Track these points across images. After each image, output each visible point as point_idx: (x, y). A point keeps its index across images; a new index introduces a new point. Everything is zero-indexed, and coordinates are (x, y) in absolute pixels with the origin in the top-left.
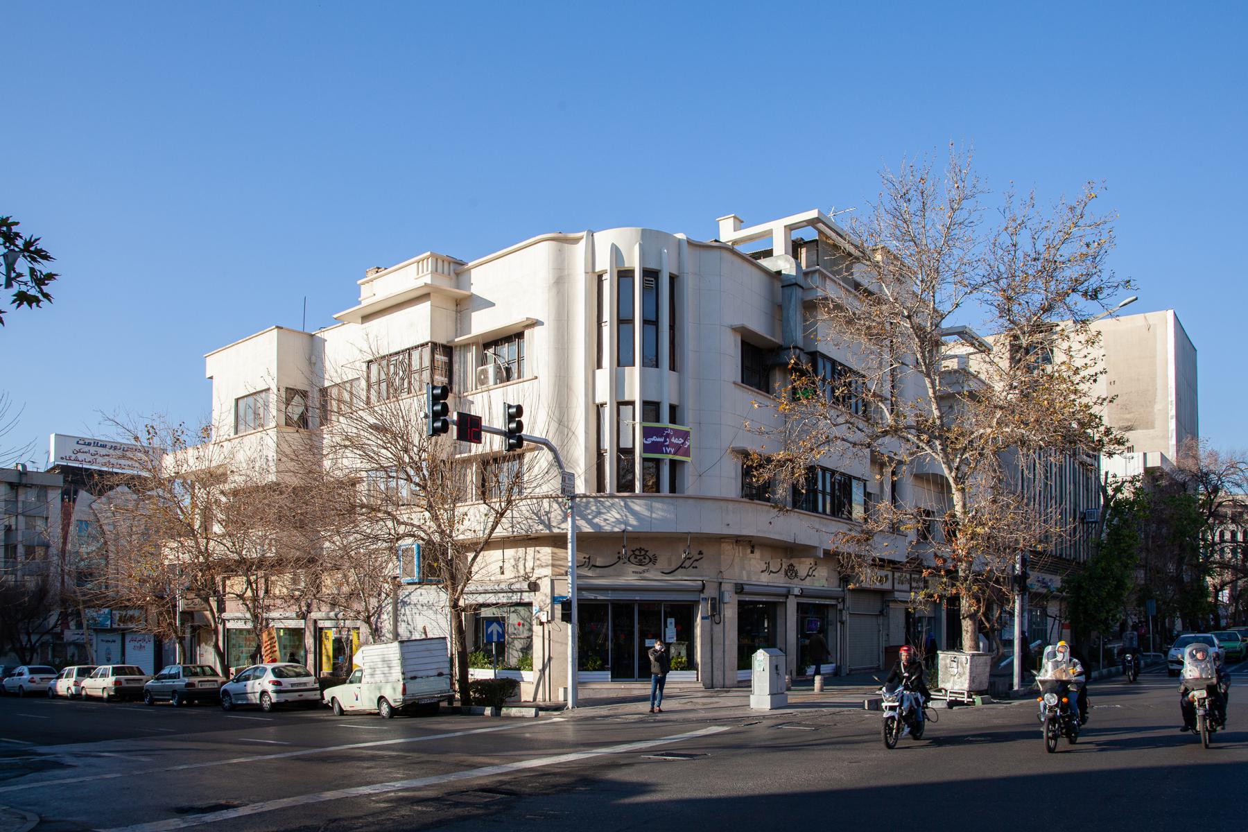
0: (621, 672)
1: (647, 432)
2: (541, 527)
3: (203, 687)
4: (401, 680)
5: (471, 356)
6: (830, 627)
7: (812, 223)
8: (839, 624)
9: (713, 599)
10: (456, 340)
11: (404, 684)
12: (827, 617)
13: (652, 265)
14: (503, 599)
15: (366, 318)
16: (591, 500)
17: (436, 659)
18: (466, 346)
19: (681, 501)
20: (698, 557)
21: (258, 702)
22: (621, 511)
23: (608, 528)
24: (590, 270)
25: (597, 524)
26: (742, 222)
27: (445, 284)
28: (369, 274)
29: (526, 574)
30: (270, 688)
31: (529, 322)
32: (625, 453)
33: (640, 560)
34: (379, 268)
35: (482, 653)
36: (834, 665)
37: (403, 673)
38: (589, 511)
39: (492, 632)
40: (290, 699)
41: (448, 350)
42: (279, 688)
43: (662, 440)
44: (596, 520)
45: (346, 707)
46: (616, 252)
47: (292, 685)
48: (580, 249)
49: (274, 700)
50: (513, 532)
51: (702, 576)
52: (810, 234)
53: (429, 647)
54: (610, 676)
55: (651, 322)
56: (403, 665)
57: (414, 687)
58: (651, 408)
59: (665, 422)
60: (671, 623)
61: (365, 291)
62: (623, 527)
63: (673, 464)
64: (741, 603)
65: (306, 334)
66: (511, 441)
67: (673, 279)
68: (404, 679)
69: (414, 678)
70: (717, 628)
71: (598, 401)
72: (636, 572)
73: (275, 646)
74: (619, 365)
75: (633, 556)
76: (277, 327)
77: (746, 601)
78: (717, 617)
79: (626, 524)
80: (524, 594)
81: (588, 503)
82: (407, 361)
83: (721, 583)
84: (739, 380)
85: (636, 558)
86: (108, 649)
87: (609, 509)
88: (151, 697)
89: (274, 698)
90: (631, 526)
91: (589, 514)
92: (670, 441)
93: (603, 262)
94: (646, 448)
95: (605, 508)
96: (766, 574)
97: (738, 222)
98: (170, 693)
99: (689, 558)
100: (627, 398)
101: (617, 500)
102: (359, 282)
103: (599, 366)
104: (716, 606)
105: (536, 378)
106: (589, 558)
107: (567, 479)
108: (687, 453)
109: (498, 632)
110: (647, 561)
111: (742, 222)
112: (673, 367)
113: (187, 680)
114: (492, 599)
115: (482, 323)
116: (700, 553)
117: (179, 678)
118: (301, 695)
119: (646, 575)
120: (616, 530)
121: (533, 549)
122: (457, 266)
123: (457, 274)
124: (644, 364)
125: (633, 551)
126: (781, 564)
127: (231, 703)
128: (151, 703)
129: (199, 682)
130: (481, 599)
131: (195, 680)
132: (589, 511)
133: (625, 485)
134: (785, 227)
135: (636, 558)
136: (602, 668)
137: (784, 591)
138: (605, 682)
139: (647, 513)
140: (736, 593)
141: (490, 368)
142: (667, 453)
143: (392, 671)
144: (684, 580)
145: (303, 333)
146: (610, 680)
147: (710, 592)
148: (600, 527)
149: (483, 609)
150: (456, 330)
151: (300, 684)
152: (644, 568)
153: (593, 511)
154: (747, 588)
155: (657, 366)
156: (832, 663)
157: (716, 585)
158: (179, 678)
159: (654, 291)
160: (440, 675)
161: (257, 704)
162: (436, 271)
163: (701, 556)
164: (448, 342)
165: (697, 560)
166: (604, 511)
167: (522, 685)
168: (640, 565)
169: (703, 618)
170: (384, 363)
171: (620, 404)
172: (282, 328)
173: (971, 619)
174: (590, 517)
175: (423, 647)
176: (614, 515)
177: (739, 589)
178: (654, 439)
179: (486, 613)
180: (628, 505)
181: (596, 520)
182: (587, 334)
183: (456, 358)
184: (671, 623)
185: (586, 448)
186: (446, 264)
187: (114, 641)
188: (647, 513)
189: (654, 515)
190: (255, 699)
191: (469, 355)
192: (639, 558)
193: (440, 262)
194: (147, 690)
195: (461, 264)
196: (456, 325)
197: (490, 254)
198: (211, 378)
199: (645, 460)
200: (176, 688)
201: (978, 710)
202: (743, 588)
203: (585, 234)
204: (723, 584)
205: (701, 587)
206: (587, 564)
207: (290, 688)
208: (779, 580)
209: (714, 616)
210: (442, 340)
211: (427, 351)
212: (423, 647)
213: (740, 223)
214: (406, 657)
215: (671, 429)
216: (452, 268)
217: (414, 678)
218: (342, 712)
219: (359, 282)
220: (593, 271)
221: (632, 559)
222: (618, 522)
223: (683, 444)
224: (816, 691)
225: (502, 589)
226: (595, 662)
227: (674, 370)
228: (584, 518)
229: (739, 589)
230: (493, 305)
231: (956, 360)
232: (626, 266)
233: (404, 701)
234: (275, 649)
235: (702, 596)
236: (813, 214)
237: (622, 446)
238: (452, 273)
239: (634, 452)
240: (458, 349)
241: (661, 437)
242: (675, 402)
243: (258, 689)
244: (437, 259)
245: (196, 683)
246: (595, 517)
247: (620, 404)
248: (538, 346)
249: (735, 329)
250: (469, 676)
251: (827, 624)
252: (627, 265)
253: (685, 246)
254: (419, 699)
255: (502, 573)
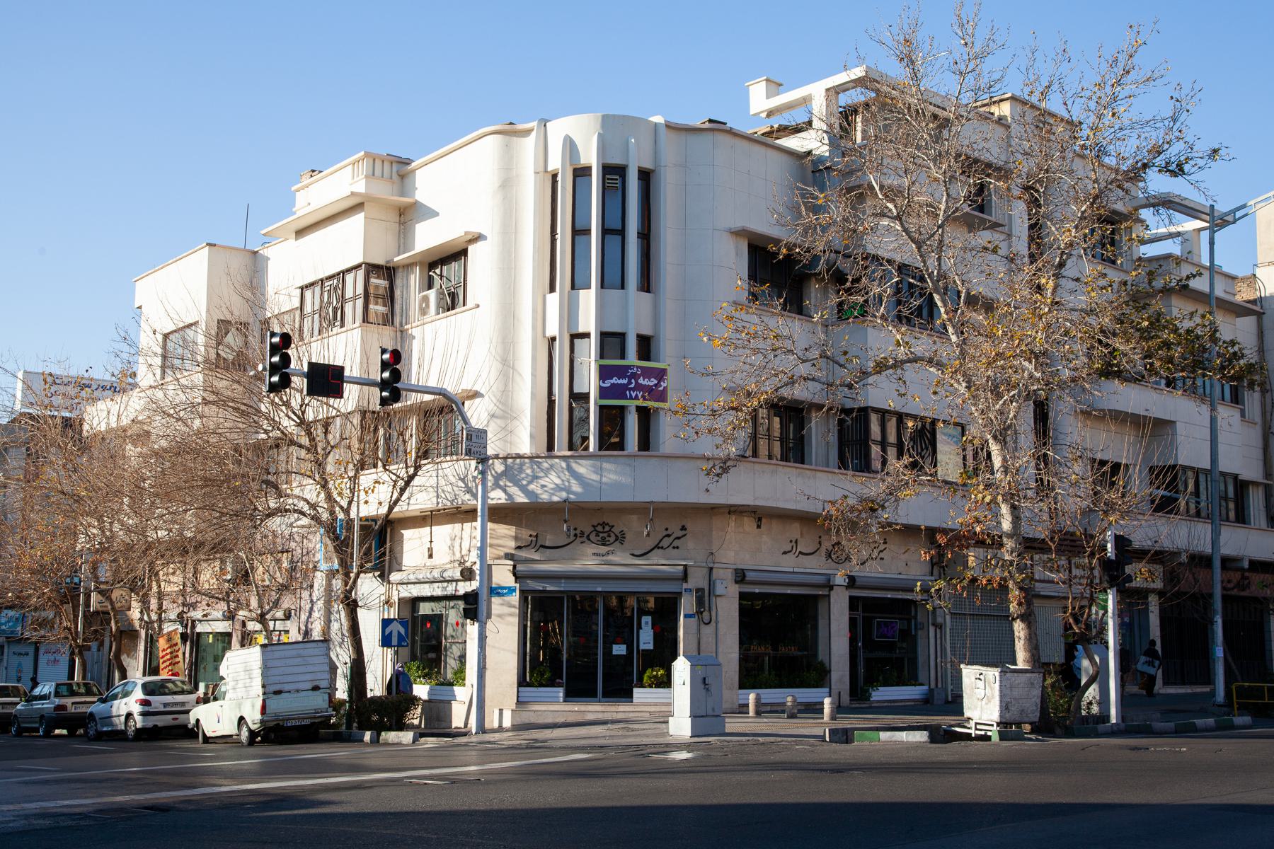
0: (579, 690)
1: (604, 373)
2: (468, 496)
3: (78, 711)
4: (261, 695)
5: (415, 278)
6: (920, 632)
7: (859, 82)
8: (932, 630)
9: (698, 590)
10: (396, 259)
11: (264, 701)
12: (915, 618)
13: (616, 160)
14: (437, 590)
15: (300, 233)
16: (527, 460)
17: (310, 669)
18: (409, 266)
19: (653, 461)
20: (680, 533)
21: (123, 728)
22: (562, 475)
23: (545, 497)
24: (542, 169)
25: (533, 492)
26: (781, 85)
27: (385, 191)
28: (303, 178)
29: (462, 557)
30: (136, 709)
31: (470, 237)
32: (579, 398)
33: (603, 538)
34: (313, 171)
35: (417, 663)
36: (925, 688)
37: (263, 686)
38: (523, 475)
39: (391, 633)
40: (160, 724)
41: (388, 272)
42: (147, 709)
43: (625, 381)
44: (532, 487)
45: (209, 734)
46: (570, 146)
47: (165, 705)
48: (529, 143)
49: (139, 725)
50: (438, 503)
51: (684, 559)
52: (856, 97)
53: (301, 651)
54: (561, 694)
55: (614, 232)
56: (264, 676)
57: (278, 705)
58: (611, 341)
59: (632, 359)
60: (647, 623)
61: (301, 199)
62: (564, 495)
63: (644, 414)
64: (743, 596)
65: (248, 251)
66: (385, 394)
67: (646, 176)
68: (264, 694)
69: (278, 692)
70: (707, 631)
71: (549, 334)
72: (598, 555)
73: (177, 656)
74: (573, 287)
75: (594, 533)
76: (209, 244)
77: (754, 593)
78: (706, 616)
79: (569, 491)
80: (459, 583)
81: (522, 465)
82: (340, 286)
83: (711, 569)
84: (744, 296)
85: (597, 535)
86: (20, 664)
87: (546, 472)
88: (19, 725)
89: (139, 722)
90: (573, 493)
91: (523, 479)
92: (636, 382)
93: (556, 162)
94: (603, 393)
95: (542, 470)
96: (791, 556)
97: (773, 87)
98: (38, 720)
99: (668, 536)
100: (581, 330)
101: (557, 460)
102: (293, 189)
103: (552, 289)
104: (704, 600)
105: (478, 306)
106: (537, 536)
107: (474, 437)
108: (662, 397)
109: (399, 632)
110: (612, 538)
111: (781, 85)
112: (646, 284)
113: (57, 701)
114: (426, 591)
115: (427, 237)
116: (683, 528)
117: (49, 699)
118: (177, 719)
119: (611, 558)
120: (556, 499)
121: (469, 524)
122: (401, 165)
123: (402, 177)
124: (603, 284)
125: (593, 526)
126: (820, 543)
127: (96, 730)
128: (19, 733)
129: (73, 703)
130: (415, 591)
131: (68, 701)
132: (523, 475)
133: (576, 443)
134: (827, 90)
135: (597, 535)
136: (551, 683)
137: (821, 580)
138: (554, 701)
139: (595, 477)
140: (736, 582)
141: (432, 294)
142: (631, 398)
143: (253, 684)
144: (660, 563)
145: (244, 250)
146: (561, 700)
147: (697, 580)
148: (537, 496)
149: (422, 604)
150: (399, 247)
151: (176, 704)
152: (606, 549)
153: (528, 475)
154: (750, 576)
155: (623, 287)
156: (923, 685)
157: (705, 571)
158: (49, 699)
159: (620, 193)
160: (316, 688)
161: (123, 731)
162: (373, 175)
163: (684, 532)
164: (388, 262)
165: (679, 538)
166: (541, 474)
167: (454, 704)
168: (603, 545)
169: (686, 616)
170: (318, 289)
171: (574, 337)
172: (215, 245)
173: (1022, 621)
174: (524, 483)
175: (294, 653)
176: (553, 480)
177: (741, 576)
178: (615, 380)
179: (425, 609)
180: (571, 468)
181: (532, 487)
182: (537, 250)
183: (398, 282)
184: (647, 623)
185: (533, 395)
186: (387, 165)
187: (27, 654)
188: (595, 477)
189: (604, 479)
190: (119, 723)
191: (412, 277)
192: (601, 535)
193: (378, 163)
194: (15, 716)
195: (407, 162)
196: (399, 236)
197: (444, 146)
198: (140, 308)
199: (602, 408)
200: (44, 713)
201: (995, 744)
202: (744, 576)
203: (535, 124)
204: (714, 570)
205: (681, 575)
206: (534, 543)
207: (162, 709)
208: (815, 566)
209: (702, 613)
210: (380, 260)
211: (361, 274)
212: (294, 653)
213: (775, 86)
214: (270, 664)
215: (638, 367)
216: (395, 169)
217: (278, 692)
218: (207, 740)
219: (293, 189)
220: (546, 171)
221: (593, 537)
222: (559, 488)
223: (656, 385)
224: (825, 719)
225: (434, 578)
226: (542, 675)
227: (648, 291)
228: (517, 483)
229: (741, 576)
230: (436, 214)
231: (1178, 240)
232: (582, 162)
233: (262, 721)
234: (177, 660)
235: (685, 586)
236: (858, 72)
237: (576, 390)
238: (395, 176)
239: (589, 397)
240: (400, 270)
241: (624, 377)
242: (647, 331)
243: (124, 712)
244: (374, 160)
245: (69, 705)
246: (530, 482)
247: (574, 337)
248: (480, 261)
249: (739, 233)
250: (368, 691)
251: (916, 628)
252: (584, 161)
253: (663, 131)
254: (283, 720)
255: (431, 556)
